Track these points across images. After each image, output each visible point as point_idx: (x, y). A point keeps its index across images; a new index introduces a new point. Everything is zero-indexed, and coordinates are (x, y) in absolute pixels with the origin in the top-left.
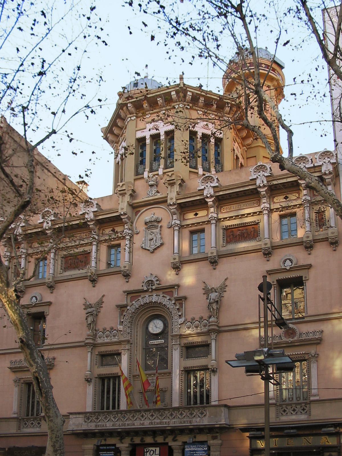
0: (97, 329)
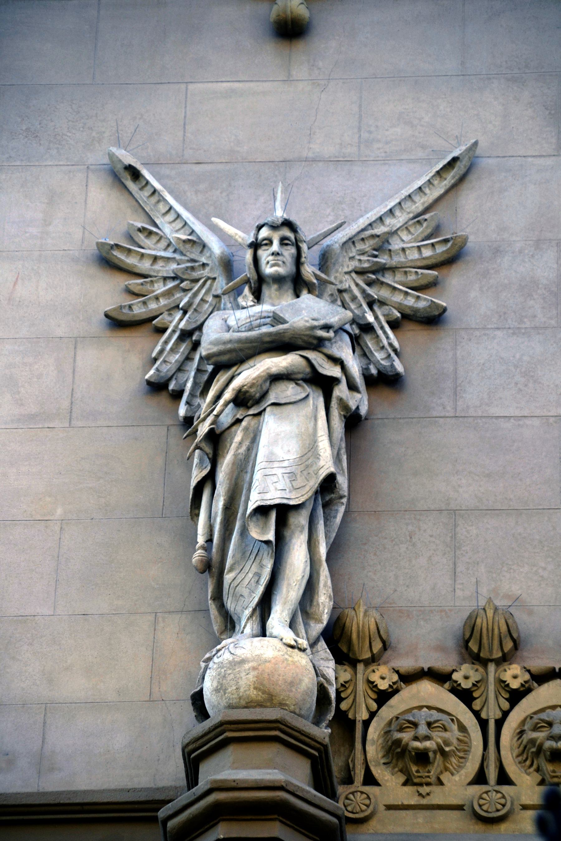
0: (361, 620)
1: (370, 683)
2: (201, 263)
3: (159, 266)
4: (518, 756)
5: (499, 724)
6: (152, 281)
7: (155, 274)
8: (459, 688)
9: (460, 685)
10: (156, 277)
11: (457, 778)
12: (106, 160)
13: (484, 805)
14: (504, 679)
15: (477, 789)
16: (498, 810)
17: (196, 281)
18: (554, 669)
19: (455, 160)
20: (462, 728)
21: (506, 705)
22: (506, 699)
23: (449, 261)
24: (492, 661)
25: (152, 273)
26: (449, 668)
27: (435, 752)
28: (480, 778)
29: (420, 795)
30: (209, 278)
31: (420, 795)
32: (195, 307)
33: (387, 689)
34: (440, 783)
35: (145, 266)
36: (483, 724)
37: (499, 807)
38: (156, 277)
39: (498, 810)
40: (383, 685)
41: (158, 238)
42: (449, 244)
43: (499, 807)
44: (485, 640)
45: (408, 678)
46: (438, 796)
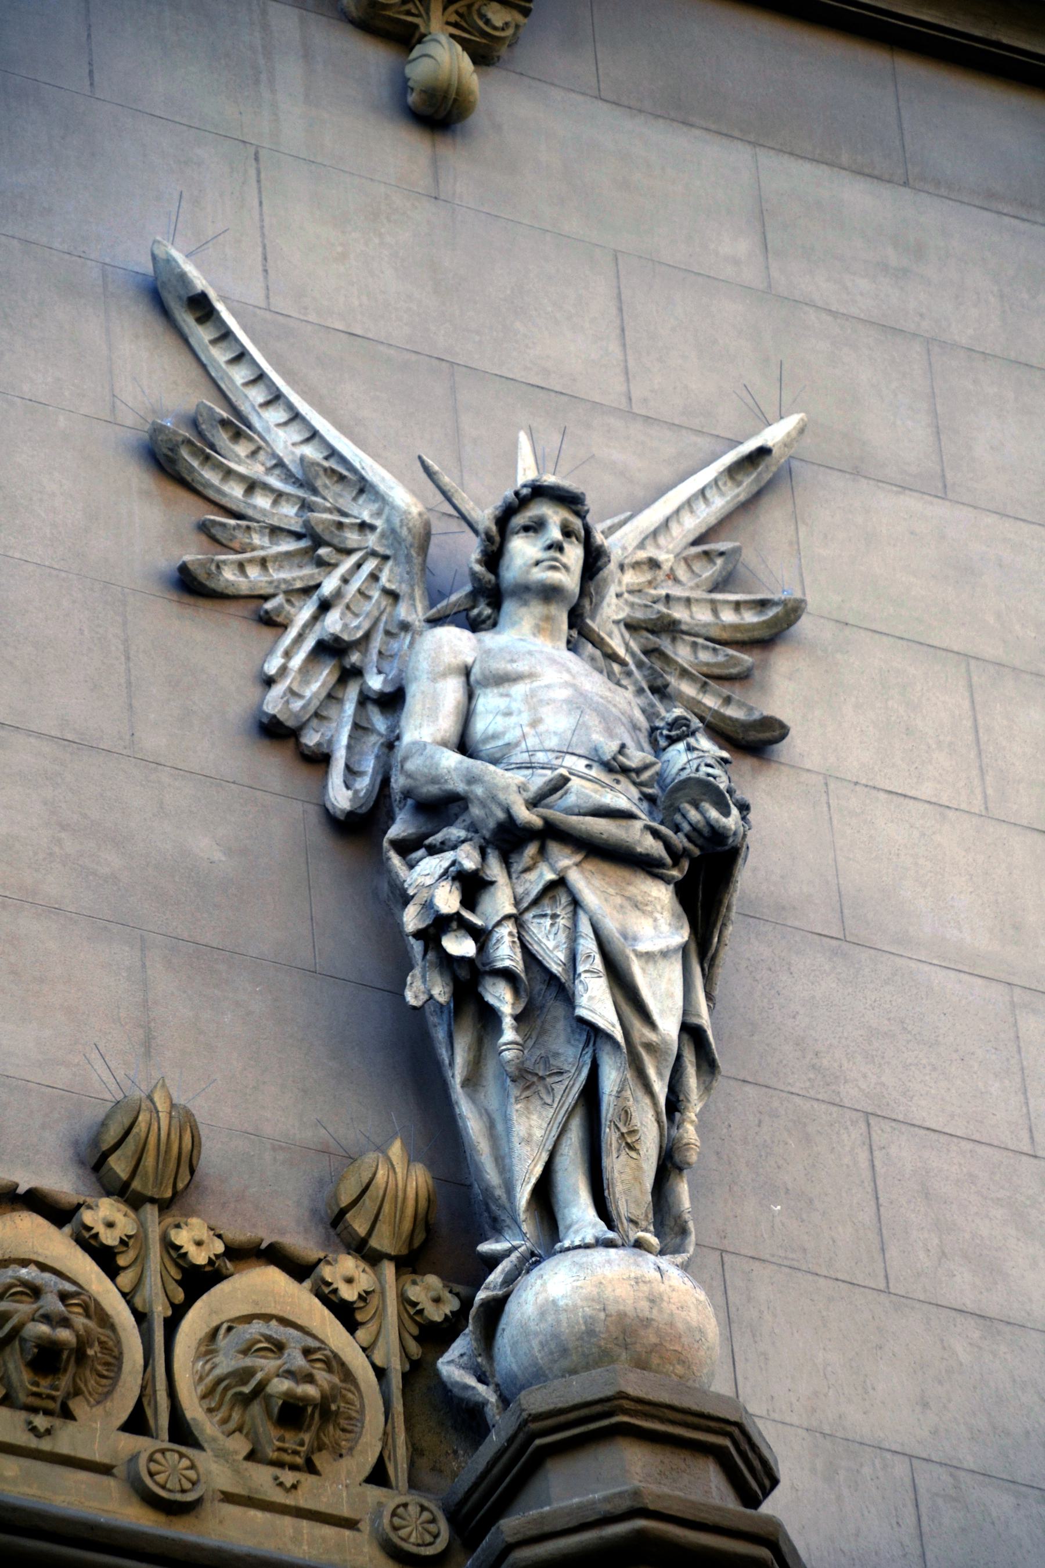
1: (170, 1247)
2: (358, 521)
3: (262, 501)
4: (204, 1397)
5: (172, 1325)
6: (248, 528)
7: (257, 516)
8: (93, 1242)
9: (335, 1291)
10: (258, 522)
11: (346, 1463)
12: (148, 268)
13: (158, 1473)
14: (178, 1243)
15: (374, 1493)
16: (183, 1491)
17: (349, 552)
18: (17, 1185)
19: (763, 452)
20: (104, 1320)
21: (180, 1296)
22: (176, 1281)
23: (765, 641)
24: (152, 1201)
25: (250, 512)
26: (75, 1199)
27: (315, 1406)
28: (137, 1423)
29: (33, 1430)
30: (374, 554)
31: (33, 1430)
32: (347, 600)
33: (204, 1266)
34: (67, 1414)
35: (235, 491)
36: (141, 1317)
37: (187, 1485)
38: (258, 522)
39: (183, 1491)
40: (199, 1257)
41: (252, 447)
42: (771, 613)
43: (187, 1485)
44: (149, 1161)
45: (243, 1254)
46: (67, 1440)
